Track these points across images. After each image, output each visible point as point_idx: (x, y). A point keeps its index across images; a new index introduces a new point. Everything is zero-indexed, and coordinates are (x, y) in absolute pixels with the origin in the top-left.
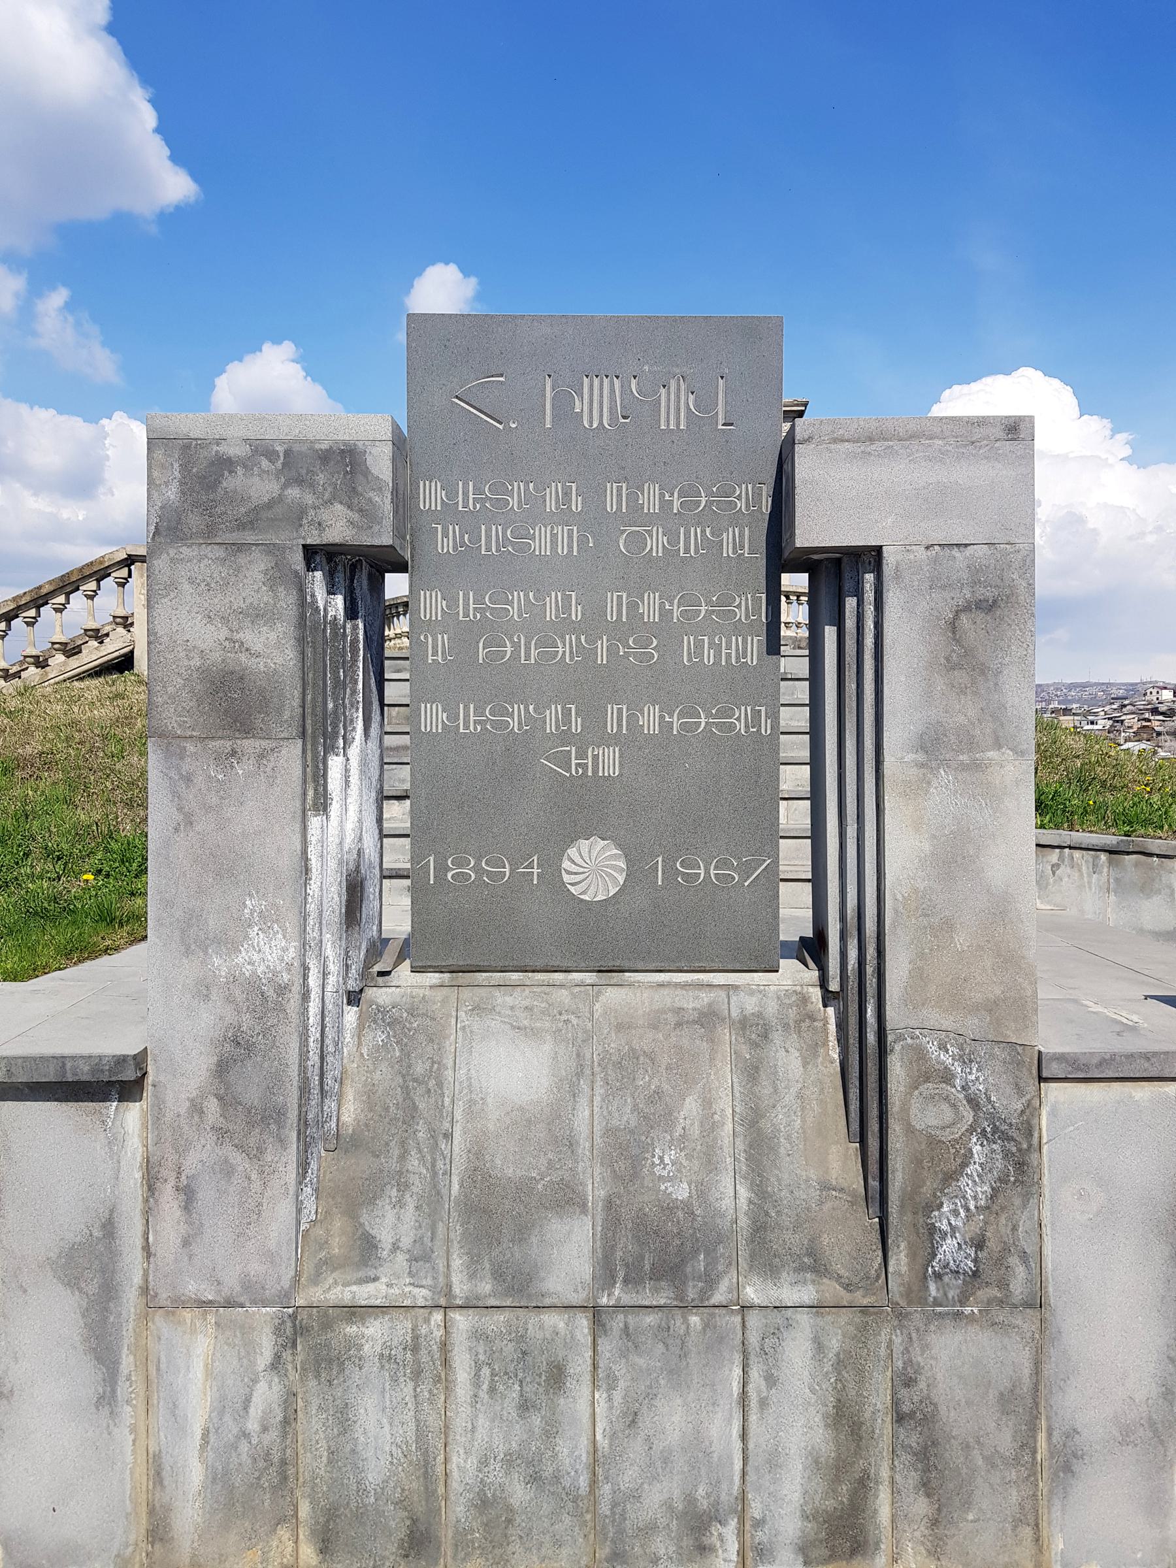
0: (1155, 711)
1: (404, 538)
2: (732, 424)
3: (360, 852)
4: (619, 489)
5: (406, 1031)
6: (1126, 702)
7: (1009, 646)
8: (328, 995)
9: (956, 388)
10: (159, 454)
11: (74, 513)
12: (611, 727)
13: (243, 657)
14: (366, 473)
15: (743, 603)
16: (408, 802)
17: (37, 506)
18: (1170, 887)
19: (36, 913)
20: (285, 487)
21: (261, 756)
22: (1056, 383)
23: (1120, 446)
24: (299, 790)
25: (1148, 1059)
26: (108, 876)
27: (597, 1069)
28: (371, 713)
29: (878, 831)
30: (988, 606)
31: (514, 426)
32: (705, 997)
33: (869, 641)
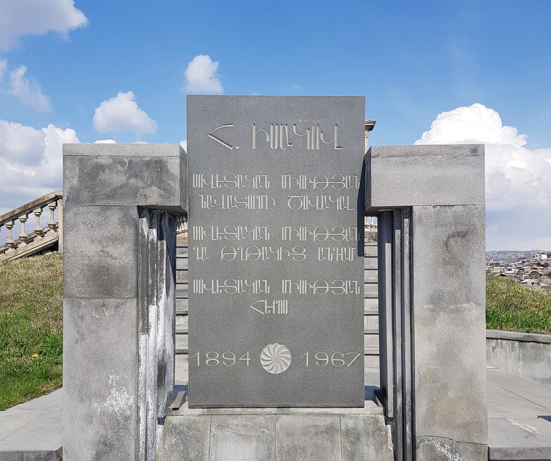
0: (539, 264)
1: (185, 202)
2: (341, 147)
3: (164, 351)
4: (288, 178)
5: (187, 437)
6: (525, 260)
7: (473, 254)
8: (149, 420)
9: (444, 113)
10: (69, 163)
11: (30, 172)
12: (284, 291)
13: (109, 260)
14: (168, 171)
15: (347, 232)
16: (187, 317)
17: (12, 169)
18: (549, 358)
19: (11, 374)
20: (129, 178)
21: (117, 307)
22: (491, 111)
23: (521, 140)
24: (135, 323)
25: (540, 451)
26: (45, 355)
27: (277, 455)
28: (169, 284)
29: (411, 341)
30: (463, 235)
31: (237, 148)
32: (329, 420)
33: (406, 251)
